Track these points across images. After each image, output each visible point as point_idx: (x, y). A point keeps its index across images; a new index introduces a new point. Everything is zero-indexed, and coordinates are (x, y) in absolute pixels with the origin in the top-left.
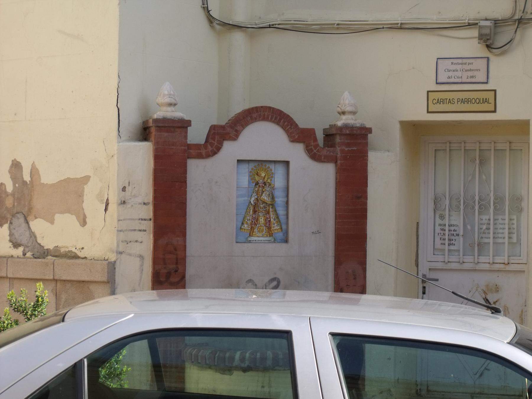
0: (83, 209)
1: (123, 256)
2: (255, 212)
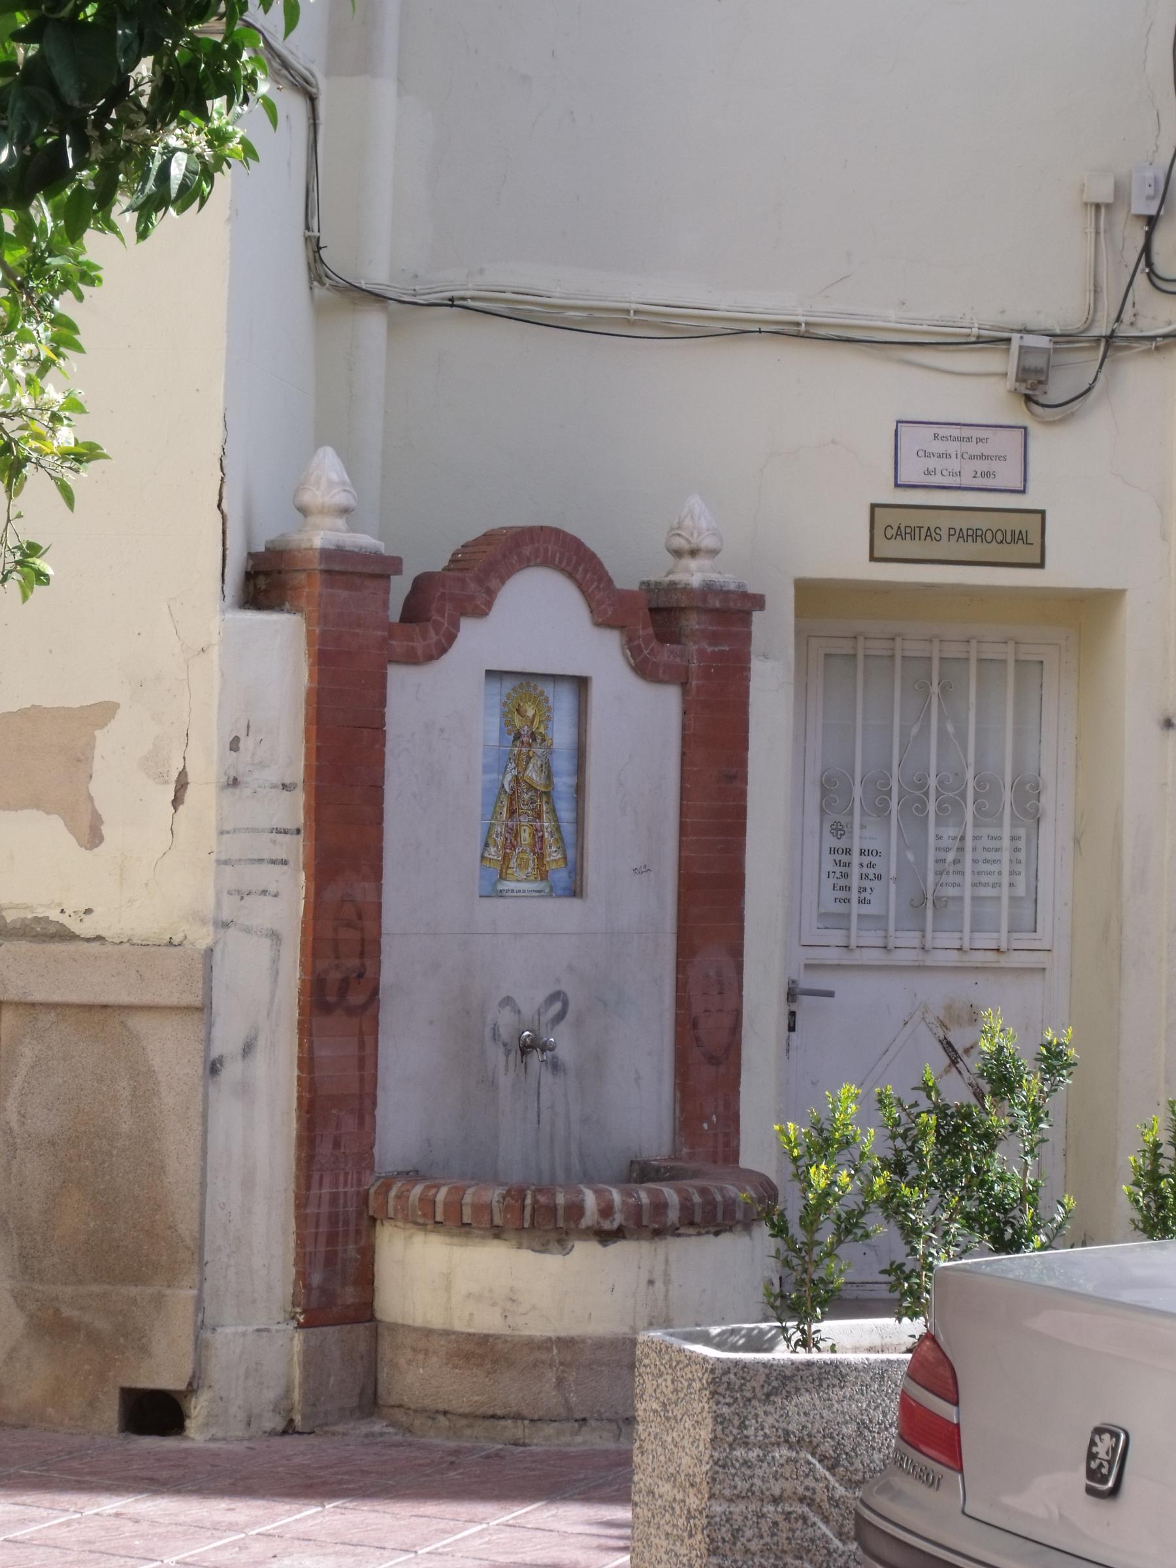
0: (91, 799)
1: (232, 932)
2: (512, 812)
